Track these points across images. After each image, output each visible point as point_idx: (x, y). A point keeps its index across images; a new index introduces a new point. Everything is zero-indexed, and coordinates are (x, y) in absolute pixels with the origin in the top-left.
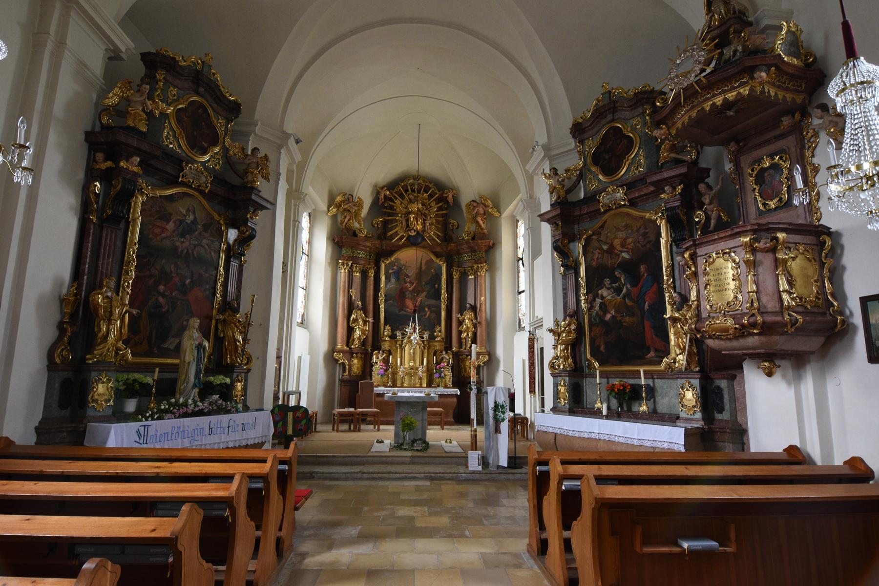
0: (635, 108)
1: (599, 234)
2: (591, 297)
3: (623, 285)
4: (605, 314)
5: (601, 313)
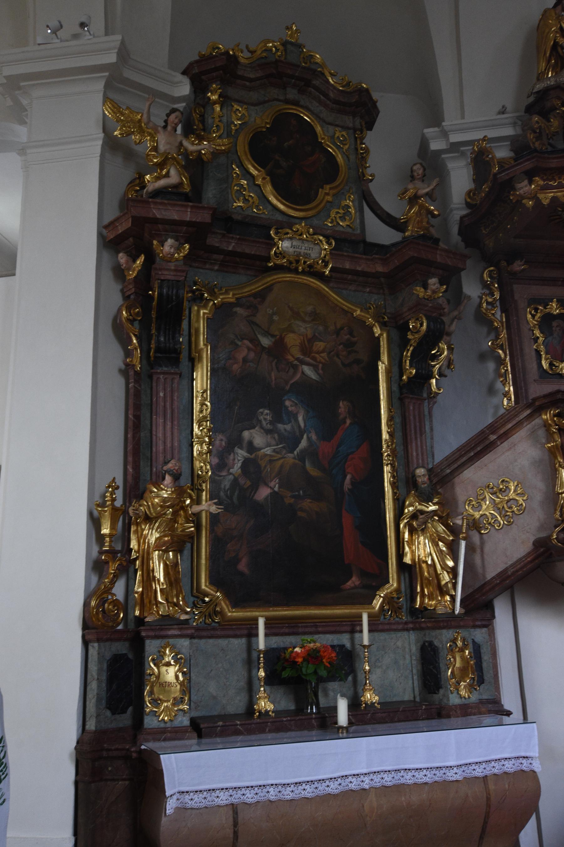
2: (221, 440)
4: (255, 487)
5: (245, 482)
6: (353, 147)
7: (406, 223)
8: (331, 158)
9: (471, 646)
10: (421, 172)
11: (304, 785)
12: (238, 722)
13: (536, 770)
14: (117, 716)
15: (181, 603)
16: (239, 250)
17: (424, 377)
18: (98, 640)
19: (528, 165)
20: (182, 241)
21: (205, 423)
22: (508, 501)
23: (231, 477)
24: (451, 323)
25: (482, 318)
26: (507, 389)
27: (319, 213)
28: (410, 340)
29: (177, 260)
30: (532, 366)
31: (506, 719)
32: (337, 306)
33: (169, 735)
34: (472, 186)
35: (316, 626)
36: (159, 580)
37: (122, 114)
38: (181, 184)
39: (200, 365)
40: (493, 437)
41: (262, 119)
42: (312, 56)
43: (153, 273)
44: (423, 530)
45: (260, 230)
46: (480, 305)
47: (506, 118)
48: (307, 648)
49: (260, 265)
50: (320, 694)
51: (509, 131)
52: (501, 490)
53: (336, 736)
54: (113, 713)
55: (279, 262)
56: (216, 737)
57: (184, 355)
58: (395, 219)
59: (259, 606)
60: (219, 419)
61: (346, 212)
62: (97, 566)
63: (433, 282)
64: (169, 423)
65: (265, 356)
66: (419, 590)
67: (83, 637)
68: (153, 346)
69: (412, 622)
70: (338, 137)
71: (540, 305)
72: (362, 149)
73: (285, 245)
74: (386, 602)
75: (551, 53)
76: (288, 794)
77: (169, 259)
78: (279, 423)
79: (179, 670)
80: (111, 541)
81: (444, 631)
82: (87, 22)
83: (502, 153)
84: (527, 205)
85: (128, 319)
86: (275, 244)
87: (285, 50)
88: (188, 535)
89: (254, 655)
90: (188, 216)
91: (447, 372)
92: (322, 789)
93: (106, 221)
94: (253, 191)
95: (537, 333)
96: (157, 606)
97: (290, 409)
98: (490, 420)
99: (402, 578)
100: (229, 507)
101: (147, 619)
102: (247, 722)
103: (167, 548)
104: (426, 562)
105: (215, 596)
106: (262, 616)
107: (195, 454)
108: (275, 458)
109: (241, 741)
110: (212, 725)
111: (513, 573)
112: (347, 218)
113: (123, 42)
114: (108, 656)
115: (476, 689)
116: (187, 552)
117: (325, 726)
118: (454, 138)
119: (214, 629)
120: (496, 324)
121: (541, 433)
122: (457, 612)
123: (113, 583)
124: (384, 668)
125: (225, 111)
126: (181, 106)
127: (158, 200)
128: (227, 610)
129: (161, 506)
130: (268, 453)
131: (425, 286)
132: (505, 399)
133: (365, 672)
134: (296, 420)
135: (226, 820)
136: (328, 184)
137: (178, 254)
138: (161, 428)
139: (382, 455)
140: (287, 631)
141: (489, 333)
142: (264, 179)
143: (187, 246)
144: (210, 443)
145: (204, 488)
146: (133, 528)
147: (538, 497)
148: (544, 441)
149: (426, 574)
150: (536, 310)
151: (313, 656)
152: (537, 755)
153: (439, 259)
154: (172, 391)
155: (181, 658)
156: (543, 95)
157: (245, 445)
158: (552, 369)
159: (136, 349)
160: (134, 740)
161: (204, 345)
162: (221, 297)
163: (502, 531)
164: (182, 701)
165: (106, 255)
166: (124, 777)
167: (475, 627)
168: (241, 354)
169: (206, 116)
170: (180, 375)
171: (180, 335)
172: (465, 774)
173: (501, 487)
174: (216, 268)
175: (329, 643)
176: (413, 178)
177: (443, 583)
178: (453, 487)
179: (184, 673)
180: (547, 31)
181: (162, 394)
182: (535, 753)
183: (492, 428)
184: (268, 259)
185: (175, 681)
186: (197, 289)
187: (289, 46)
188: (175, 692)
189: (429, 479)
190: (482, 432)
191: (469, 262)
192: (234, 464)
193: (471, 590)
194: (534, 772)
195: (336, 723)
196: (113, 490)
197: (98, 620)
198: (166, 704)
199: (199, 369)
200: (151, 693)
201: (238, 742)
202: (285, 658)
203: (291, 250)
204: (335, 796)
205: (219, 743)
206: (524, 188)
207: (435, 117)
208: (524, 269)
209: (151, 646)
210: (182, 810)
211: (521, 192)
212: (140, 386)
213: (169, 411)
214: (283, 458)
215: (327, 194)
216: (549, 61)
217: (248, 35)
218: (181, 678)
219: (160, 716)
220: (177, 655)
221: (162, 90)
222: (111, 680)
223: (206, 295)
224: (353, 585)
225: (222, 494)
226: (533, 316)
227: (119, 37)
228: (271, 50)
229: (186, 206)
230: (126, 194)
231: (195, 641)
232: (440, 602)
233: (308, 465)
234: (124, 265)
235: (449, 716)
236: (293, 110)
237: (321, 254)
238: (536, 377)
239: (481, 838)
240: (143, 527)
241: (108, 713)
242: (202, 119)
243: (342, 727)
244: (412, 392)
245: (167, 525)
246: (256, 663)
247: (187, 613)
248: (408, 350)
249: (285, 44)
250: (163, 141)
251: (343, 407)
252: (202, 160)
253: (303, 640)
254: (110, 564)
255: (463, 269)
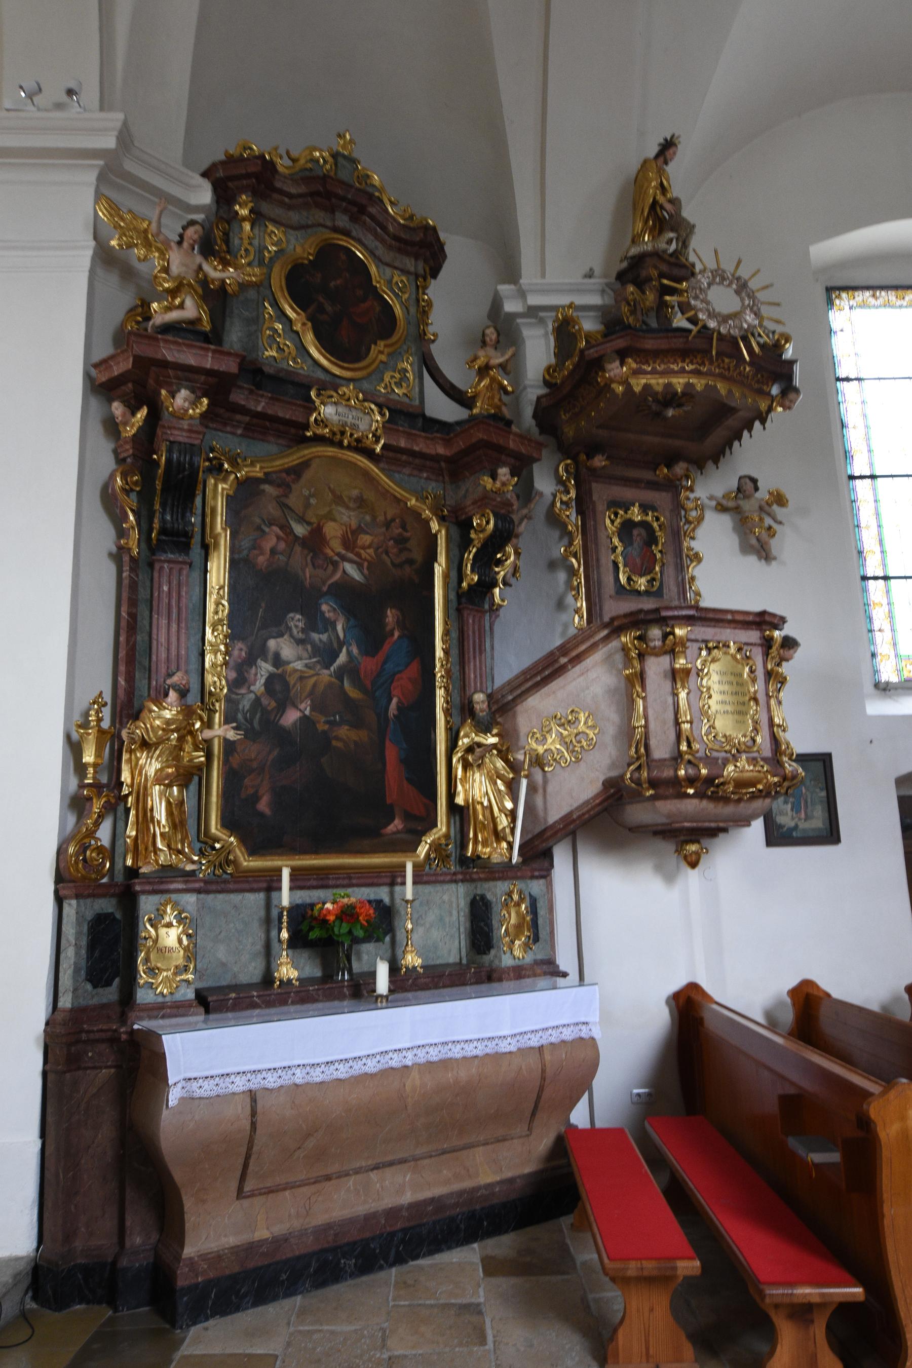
0: (400, 251)
1: (286, 487)
2: (240, 650)
3: (341, 644)
4: (281, 708)
5: (269, 703)
6: (414, 296)
7: (474, 398)
8: (387, 308)
9: (528, 899)
10: (494, 337)
11: (337, 1064)
12: (255, 994)
13: (596, 1037)
14: (100, 990)
15: (187, 850)
16: (270, 412)
17: (486, 585)
18: (77, 897)
19: (620, 343)
20: (199, 394)
21: (220, 628)
22: (577, 735)
23: (252, 696)
24: (520, 523)
25: (554, 520)
26: (579, 605)
27: (370, 375)
28: (472, 540)
29: (191, 417)
30: (609, 580)
31: (560, 981)
32: (388, 491)
33: (169, 1011)
34: (553, 361)
35: (350, 878)
36: (159, 822)
37: (122, 219)
38: (199, 320)
39: (216, 554)
40: (563, 660)
41: (303, 248)
42: (368, 176)
43: (159, 432)
44: (479, 766)
45: (298, 389)
46: (553, 504)
47: (594, 284)
48: (340, 904)
49: (296, 433)
50: (353, 958)
51: (595, 300)
52: (569, 721)
53: (373, 1006)
54: (95, 987)
55: (319, 431)
56: (226, 1011)
57: (197, 539)
58: (460, 391)
59: (280, 854)
60: (239, 624)
61: (401, 380)
62: (76, 804)
63: (503, 472)
64: (174, 627)
65: (298, 549)
66: (471, 835)
67: (56, 892)
68: (156, 525)
69: (462, 873)
70: (397, 283)
71: (621, 509)
72: (423, 300)
73: (328, 411)
74: (433, 849)
75: (649, 213)
76: (317, 1076)
77: (180, 416)
78: (314, 631)
79: (184, 932)
80: (95, 772)
81: (499, 883)
82: (77, 89)
83: (589, 325)
84: (617, 391)
85: (123, 489)
86: (315, 409)
87: (336, 164)
88: (196, 767)
89: (275, 913)
90: (208, 363)
91: (512, 581)
92: (358, 1068)
93: (96, 358)
94: (289, 339)
95: (616, 541)
96: (155, 854)
97: (327, 615)
98: (558, 642)
99: (452, 821)
100: (250, 734)
101: (142, 870)
102: (266, 993)
103: (171, 781)
104: (482, 804)
105: (227, 841)
106: (287, 866)
107: (207, 665)
108: (307, 675)
109: (257, 1016)
110: (222, 997)
111: (579, 817)
112: (404, 384)
113: (125, 123)
114: (89, 915)
115: (531, 949)
116: (193, 787)
117: (360, 992)
118: (534, 300)
119: (225, 882)
120: (570, 528)
121: (619, 658)
122: (514, 861)
123: (97, 824)
124: (428, 925)
125: (256, 231)
126: (199, 217)
127: (170, 338)
128: (242, 859)
129: (163, 730)
130: (299, 667)
131: (494, 477)
132: (577, 616)
133: (407, 932)
134: (334, 629)
135: (242, 1110)
136: (382, 338)
137: (194, 410)
138: (163, 631)
139: (434, 675)
140: (315, 883)
141: (561, 538)
142: (304, 324)
143: (205, 401)
144: (227, 653)
145: (218, 708)
146: (125, 756)
147: (611, 730)
148: (621, 666)
149: (481, 817)
150: (616, 514)
151: (348, 914)
152: (598, 1020)
153: (512, 445)
154: (179, 585)
155: (186, 918)
156: (637, 262)
157: (270, 656)
158: (629, 584)
159: (133, 528)
160: (123, 1018)
161: (222, 528)
162: (246, 469)
163: (569, 768)
164: (186, 969)
165: (94, 402)
166: (109, 1063)
167: (533, 877)
168: (270, 543)
169: (231, 234)
170: (190, 565)
171: (192, 514)
172: (519, 1045)
173: (570, 717)
174: (239, 432)
175: (365, 897)
176: (484, 343)
177: (500, 827)
178: (514, 716)
179: (189, 936)
180: (646, 185)
181: (165, 588)
182: (594, 1017)
183: (563, 649)
184: (307, 427)
185: (178, 945)
186: (215, 458)
187: (340, 160)
188: (177, 959)
189: (489, 705)
190: (552, 653)
191: (545, 452)
192: (255, 680)
193: (530, 836)
194: (593, 1039)
195: (375, 991)
196: (100, 708)
197: (77, 870)
198: (165, 974)
199: (215, 559)
200: (147, 960)
201: (253, 1017)
202: (312, 916)
203: (336, 418)
204: (373, 1076)
205: (230, 1019)
206: (615, 370)
207: (510, 271)
208: (604, 467)
209: (147, 904)
210: (188, 1100)
211: (612, 374)
212: (137, 576)
213: (175, 610)
214: (318, 674)
215: (381, 352)
216: (646, 221)
217: (292, 138)
218: (185, 942)
219: (157, 988)
220: (180, 914)
221: (173, 193)
222: (92, 946)
223: (226, 466)
224: (395, 829)
225: (240, 716)
226: (612, 522)
227: (120, 116)
228: (318, 161)
229: (207, 349)
230: (123, 325)
231: (202, 896)
232: (495, 849)
233: (346, 684)
234: (120, 418)
235: (500, 980)
236: (343, 242)
237: (371, 426)
238: (613, 592)
239: (533, 1114)
240: (138, 755)
241: (89, 986)
242: (227, 240)
243: (381, 996)
244: (473, 601)
245: (171, 753)
246: (277, 923)
247: (193, 862)
248: (470, 552)
249: (335, 156)
250: (179, 262)
251: (391, 616)
252: (225, 291)
253: (334, 895)
254: (94, 801)
255: (538, 460)
